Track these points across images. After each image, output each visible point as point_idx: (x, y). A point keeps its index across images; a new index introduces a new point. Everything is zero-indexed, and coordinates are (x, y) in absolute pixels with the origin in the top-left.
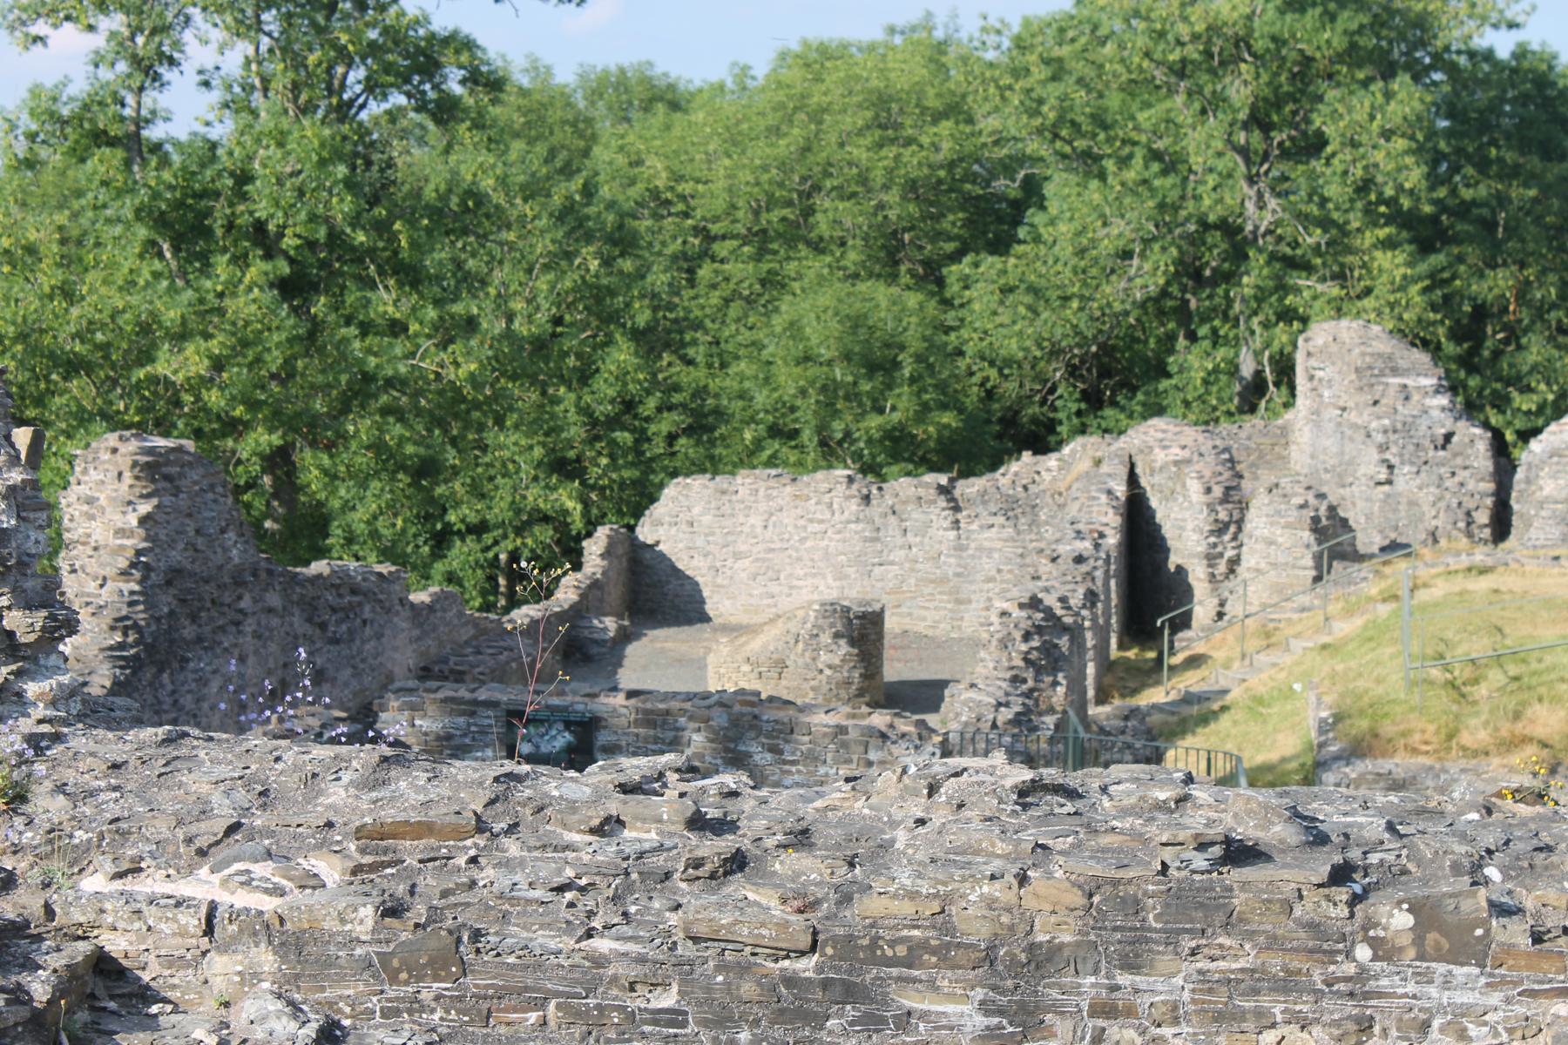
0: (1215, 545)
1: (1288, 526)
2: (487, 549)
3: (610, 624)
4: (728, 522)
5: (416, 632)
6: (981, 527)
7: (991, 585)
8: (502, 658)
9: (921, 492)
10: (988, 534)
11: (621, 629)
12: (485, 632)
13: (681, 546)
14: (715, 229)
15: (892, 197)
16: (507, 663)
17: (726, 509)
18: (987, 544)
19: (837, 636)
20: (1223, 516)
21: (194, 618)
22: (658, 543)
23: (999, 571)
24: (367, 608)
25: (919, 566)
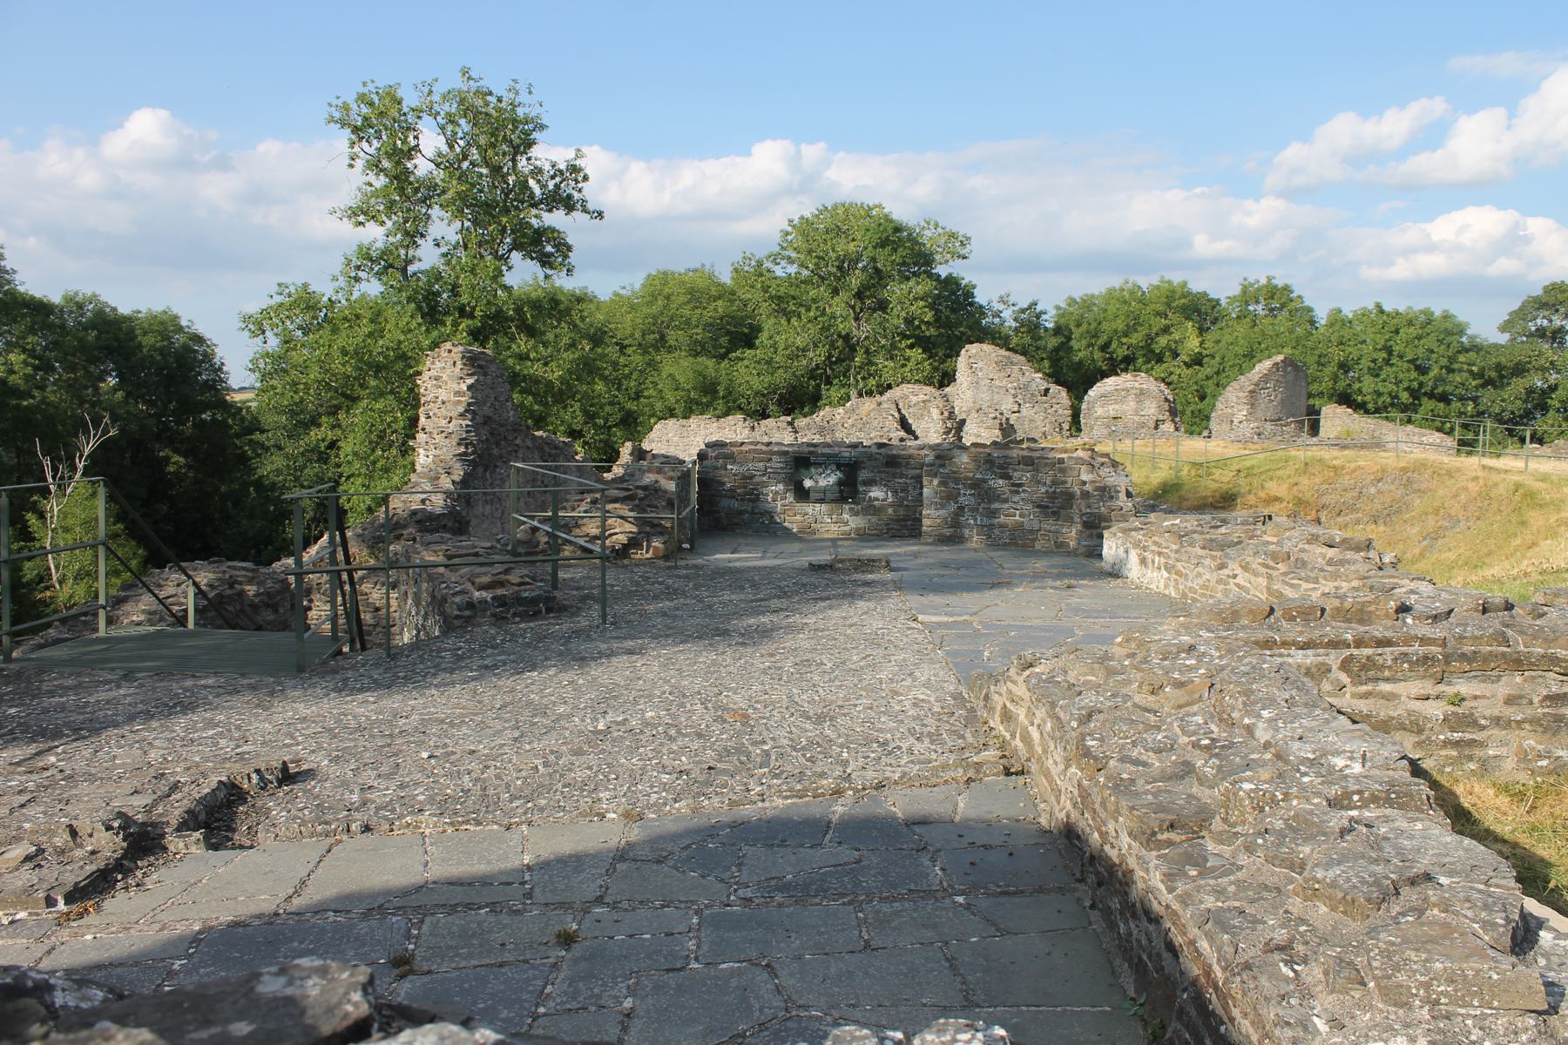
1: (987, 428)
15: (699, 331)
17: (685, 434)
20: (949, 425)
21: (497, 444)
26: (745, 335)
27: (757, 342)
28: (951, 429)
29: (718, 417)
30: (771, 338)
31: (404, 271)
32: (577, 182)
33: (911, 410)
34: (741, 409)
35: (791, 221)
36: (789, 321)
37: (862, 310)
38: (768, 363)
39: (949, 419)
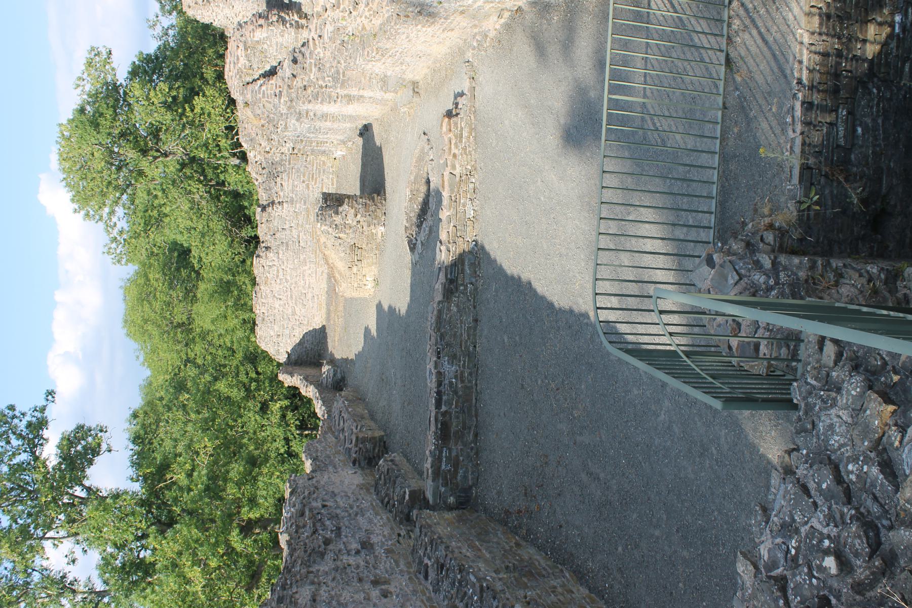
0: (291, 24)
2: (295, 437)
3: (325, 368)
4: (278, 318)
5: (331, 469)
6: (282, 190)
7: (310, 186)
8: (346, 416)
9: (264, 220)
10: (285, 187)
11: (328, 363)
12: (330, 428)
13: (289, 341)
14: (184, 357)
16: (349, 413)
17: (271, 318)
18: (290, 188)
19: (337, 213)
20: (275, 18)
22: (287, 352)
23: (303, 182)
24: (314, 504)
25: (300, 223)
26: (179, 255)
27: (185, 245)
28: (280, 17)
29: (254, 282)
30: (181, 233)
31: (102, 594)
32: (14, 417)
33: (255, 66)
34: (244, 261)
35: (75, 211)
36: (166, 215)
37: (158, 151)
38: (203, 235)
39: (267, 18)
